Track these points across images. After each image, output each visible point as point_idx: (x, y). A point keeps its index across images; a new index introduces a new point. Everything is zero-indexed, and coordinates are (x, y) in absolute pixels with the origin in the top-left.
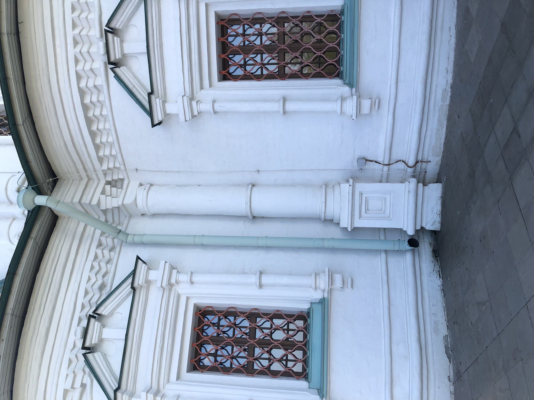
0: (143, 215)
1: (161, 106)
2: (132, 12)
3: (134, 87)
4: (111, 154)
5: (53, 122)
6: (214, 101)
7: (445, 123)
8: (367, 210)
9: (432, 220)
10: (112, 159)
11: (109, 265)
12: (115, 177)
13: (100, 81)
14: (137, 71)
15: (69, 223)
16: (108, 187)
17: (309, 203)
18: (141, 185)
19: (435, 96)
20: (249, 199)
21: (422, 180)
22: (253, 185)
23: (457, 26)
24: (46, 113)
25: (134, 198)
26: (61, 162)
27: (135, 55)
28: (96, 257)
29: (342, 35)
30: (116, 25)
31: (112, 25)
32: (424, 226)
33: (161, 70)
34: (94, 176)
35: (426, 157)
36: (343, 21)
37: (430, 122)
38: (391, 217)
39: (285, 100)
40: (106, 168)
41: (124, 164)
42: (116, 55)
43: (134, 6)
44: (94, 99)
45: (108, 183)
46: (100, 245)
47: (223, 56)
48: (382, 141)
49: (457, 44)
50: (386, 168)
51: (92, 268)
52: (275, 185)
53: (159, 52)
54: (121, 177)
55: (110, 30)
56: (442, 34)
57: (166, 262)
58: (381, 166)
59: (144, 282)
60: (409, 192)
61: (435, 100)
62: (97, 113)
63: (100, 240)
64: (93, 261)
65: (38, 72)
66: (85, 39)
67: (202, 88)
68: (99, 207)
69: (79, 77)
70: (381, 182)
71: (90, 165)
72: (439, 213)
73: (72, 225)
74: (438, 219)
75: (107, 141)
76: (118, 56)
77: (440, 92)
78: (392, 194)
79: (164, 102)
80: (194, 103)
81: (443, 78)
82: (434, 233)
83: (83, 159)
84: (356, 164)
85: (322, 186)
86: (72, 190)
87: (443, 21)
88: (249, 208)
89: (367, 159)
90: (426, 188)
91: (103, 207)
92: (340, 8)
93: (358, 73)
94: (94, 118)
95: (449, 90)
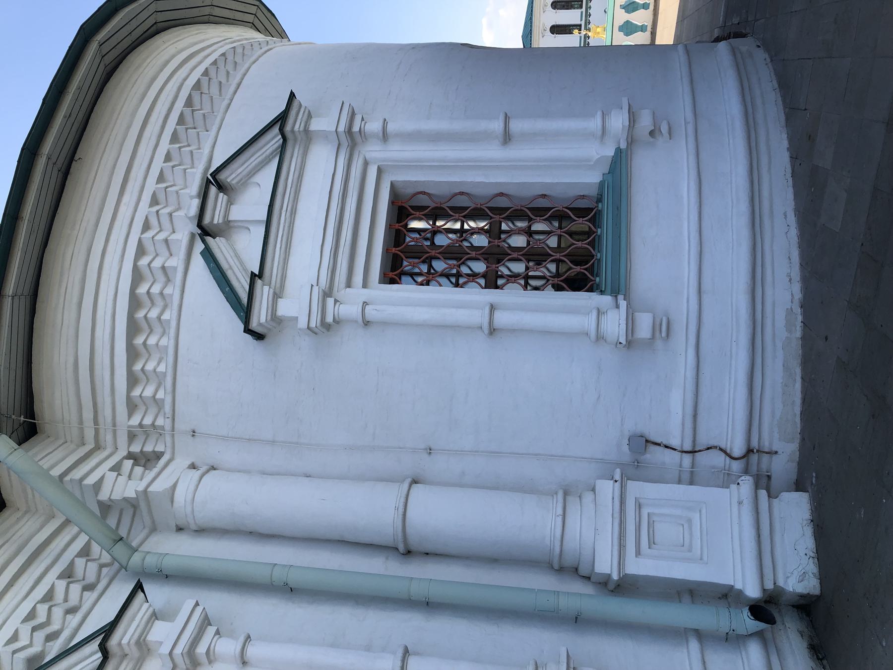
0: (180, 529)
1: (270, 303)
2: (260, 163)
3: (231, 268)
4: (154, 396)
5: (70, 315)
6: (365, 304)
7: (798, 371)
8: (652, 543)
9: (797, 571)
10: (153, 411)
11: (69, 617)
12: (149, 448)
13: (176, 262)
14: (242, 251)
15: (25, 519)
16: (129, 463)
17: (529, 521)
18: (193, 466)
19: (774, 320)
20: (403, 500)
21: (764, 482)
22: (415, 482)
23: (797, 211)
24: (62, 299)
25: (171, 483)
26: (57, 397)
27: (245, 226)
28: (48, 597)
29: (599, 230)
30: (227, 178)
31: (222, 176)
32: (781, 583)
33: (283, 246)
34: (109, 437)
35: (767, 444)
36: (599, 260)
37: (769, 361)
38: (705, 558)
39: (493, 308)
40: (137, 423)
41: (174, 419)
42: (214, 216)
43: (264, 156)
44: (156, 290)
45: (130, 456)
46: (68, 574)
47: (397, 226)
48: (677, 402)
49: (802, 236)
50: (687, 460)
51: (32, 615)
52: (458, 483)
53: (288, 220)
54: (160, 448)
55: (215, 182)
56: (772, 222)
57: (197, 604)
58: (677, 455)
59: (133, 641)
60: (740, 503)
61: (774, 331)
62: (153, 314)
63: (72, 564)
64: (38, 602)
65: (76, 232)
66: (172, 199)
67: (349, 285)
68: (97, 494)
69: (141, 251)
70: (680, 482)
71: (108, 412)
72: (812, 555)
73: (27, 526)
74: (812, 567)
75: (155, 370)
76: (218, 219)
77: (781, 321)
78: (704, 511)
79: (277, 296)
80: (330, 301)
81: (785, 291)
82: (805, 607)
83: (99, 400)
84: (626, 448)
85: (556, 493)
86: (58, 454)
87: (771, 195)
88: (401, 517)
89: (649, 439)
90: (775, 502)
91: (104, 496)
92: (594, 192)
93: (628, 273)
94: (143, 351)
95: (798, 310)
